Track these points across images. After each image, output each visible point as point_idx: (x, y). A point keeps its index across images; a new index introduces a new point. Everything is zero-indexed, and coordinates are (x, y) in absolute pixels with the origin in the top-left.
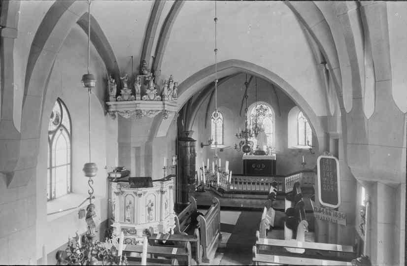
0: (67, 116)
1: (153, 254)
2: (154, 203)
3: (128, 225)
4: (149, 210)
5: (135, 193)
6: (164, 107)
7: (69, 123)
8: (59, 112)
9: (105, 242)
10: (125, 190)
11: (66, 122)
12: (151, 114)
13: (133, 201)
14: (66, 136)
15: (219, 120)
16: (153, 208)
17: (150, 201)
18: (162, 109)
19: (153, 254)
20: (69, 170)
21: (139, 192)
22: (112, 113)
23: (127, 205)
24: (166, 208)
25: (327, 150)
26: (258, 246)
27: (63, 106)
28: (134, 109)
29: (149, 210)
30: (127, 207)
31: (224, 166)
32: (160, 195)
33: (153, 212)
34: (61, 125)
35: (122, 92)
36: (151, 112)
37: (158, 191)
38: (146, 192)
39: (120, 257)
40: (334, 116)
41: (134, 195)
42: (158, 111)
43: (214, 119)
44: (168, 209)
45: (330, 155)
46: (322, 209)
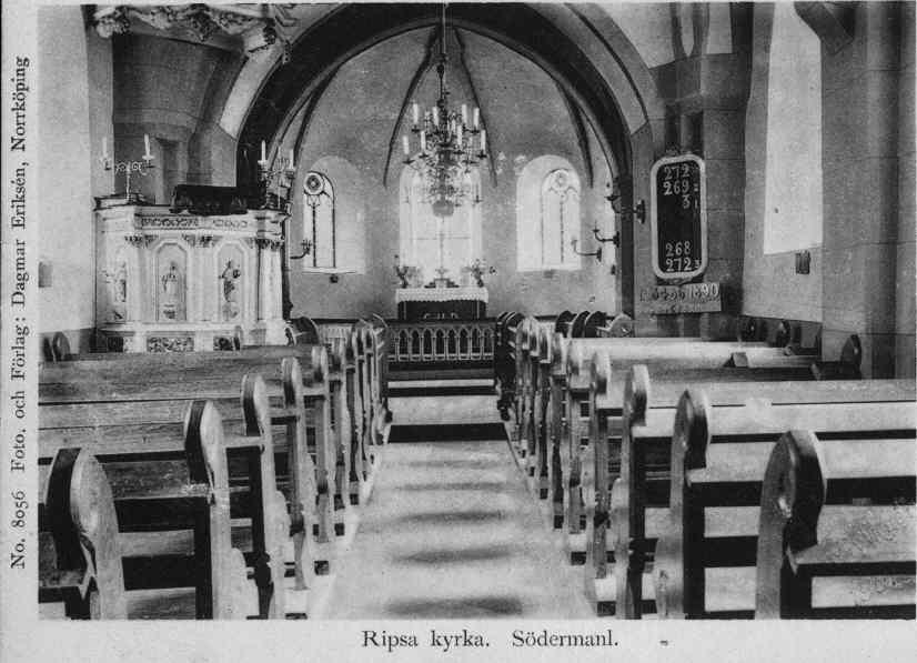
1: (392, 385)
4: (229, 287)
5: (190, 239)
10: (157, 232)
12: (230, 21)
13: (180, 263)
17: (229, 265)
19: (392, 385)
21: (199, 233)
22: (170, 482)
25: (672, 142)
26: (554, 376)
29: (229, 287)
31: (465, 139)
32: (254, 251)
36: (231, 17)
37: (248, 241)
38: (218, 239)
39: (572, 405)
40: (692, 56)
41: (187, 247)
45: (684, 153)
46: (661, 288)
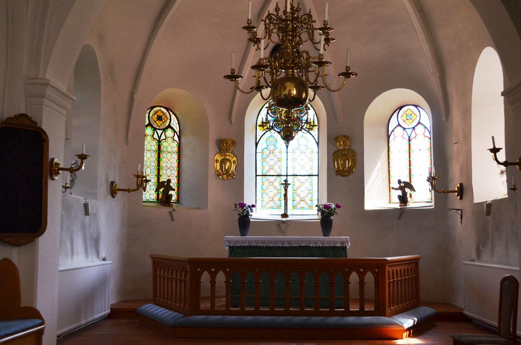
15: (169, 133)
43: (155, 129)
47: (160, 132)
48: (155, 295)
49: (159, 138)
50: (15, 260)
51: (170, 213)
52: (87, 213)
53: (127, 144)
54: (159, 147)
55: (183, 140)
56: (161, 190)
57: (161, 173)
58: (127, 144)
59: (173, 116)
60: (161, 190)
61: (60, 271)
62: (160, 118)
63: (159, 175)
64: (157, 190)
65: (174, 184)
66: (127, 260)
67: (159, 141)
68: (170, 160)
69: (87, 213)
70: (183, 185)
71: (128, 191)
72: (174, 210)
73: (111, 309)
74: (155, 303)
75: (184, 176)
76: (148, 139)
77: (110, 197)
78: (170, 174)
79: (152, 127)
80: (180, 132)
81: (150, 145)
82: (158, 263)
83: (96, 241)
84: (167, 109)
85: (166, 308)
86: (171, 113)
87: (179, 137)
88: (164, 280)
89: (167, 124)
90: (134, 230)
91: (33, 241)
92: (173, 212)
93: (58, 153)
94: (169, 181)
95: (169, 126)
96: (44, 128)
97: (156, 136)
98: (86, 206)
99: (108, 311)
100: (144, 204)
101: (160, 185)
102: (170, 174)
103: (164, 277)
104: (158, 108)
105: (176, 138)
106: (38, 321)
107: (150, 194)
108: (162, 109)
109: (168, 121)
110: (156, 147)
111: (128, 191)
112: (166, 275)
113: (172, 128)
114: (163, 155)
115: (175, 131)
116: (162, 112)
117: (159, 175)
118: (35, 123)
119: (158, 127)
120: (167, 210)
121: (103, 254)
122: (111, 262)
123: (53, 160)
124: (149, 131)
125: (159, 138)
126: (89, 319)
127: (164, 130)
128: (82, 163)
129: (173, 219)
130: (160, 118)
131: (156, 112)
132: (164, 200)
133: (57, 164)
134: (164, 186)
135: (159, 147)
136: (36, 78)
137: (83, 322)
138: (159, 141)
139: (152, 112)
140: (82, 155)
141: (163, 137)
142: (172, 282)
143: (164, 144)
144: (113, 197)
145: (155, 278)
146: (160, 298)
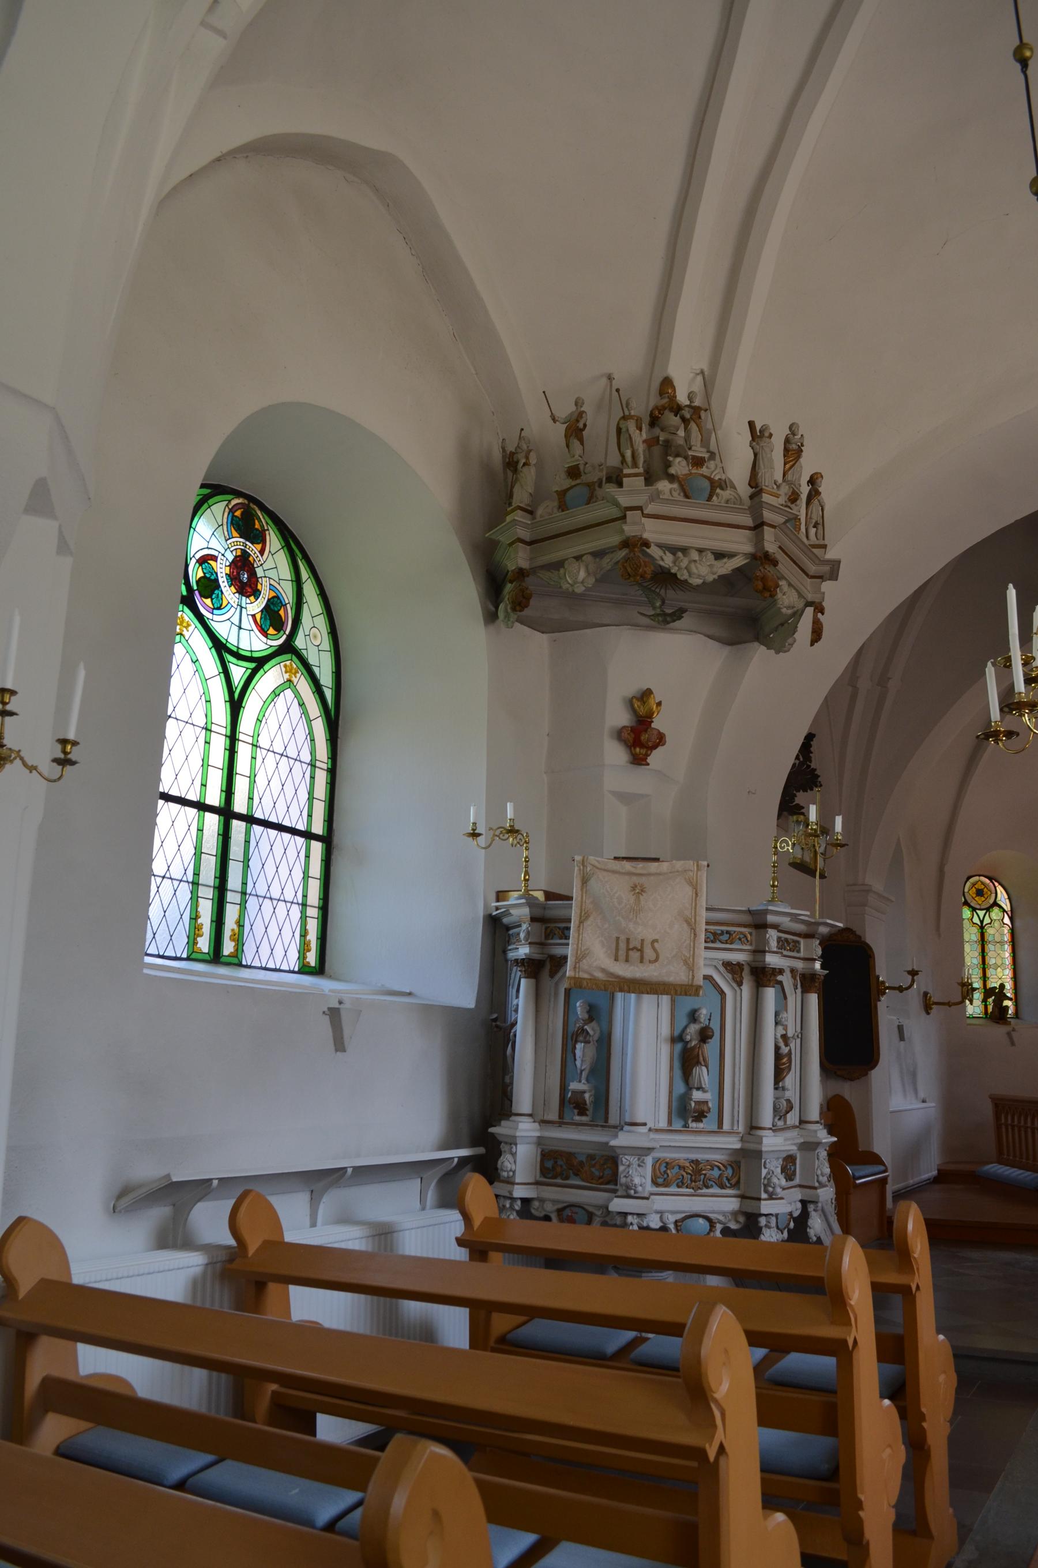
0: (322, 622)
2: (715, 1026)
3: (578, 1136)
6: (759, 540)
7: (326, 644)
8: (288, 594)
9: (764, 1419)
11: (313, 638)
14: (314, 708)
15: (996, 913)
16: (710, 1049)
18: (749, 548)
20: (316, 868)
23: (572, 1028)
24: (779, 1074)
27: (305, 574)
28: (615, 540)
30: (580, 1034)
32: (746, 989)
33: (703, 1075)
34: (288, 648)
35: (789, 1115)
42: (731, 555)
43: (974, 909)
44: (790, 1080)
47: (981, 913)
48: (1000, 1152)
49: (982, 922)
50: (847, 1097)
51: (1009, 1034)
52: (902, 1038)
53: (939, 935)
54: (982, 935)
55: (1017, 923)
56: (991, 1000)
57: (988, 974)
58: (939, 935)
59: (1000, 889)
60: (991, 1000)
61: (892, 1112)
62: (980, 893)
63: (985, 978)
64: (985, 1000)
65: (1009, 986)
66: (952, 1104)
67: (982, 927)
68: (1001, 956)
69: (902, 1038)
70: (1024, 990)
71: (949, 1004)
72: (1014, 1030)
73: (939, 1170)
74: (1000, 1163)
75: (1023, 978)
76: (966, 924)
77: (924, 1013)
78: (1002, 976)
79: (969, 906)
80: (1012, 910)
81: (971, 934)
82: (1002, 1106)
83: (914, 1075)
84: (990, 879)
85: (1020, 1168)
86: (996, 884)
87: (1011, 919)
88: (1013, 1130)
89: (991, 901)
90: (958, 1061)
91: (866, 1074)
92: (1014, 1034)
93: (884, 971)
94: (1002, 986)
95: (995, 904)
96: (868, 941)
97: (976, 920)
98: (900, 1028)
99: (935, 1173)
100: (969, 1021)
101: (988, 992)
102: (1002, 976)
103: (1013, 1127)
104: (976, 878)
105: (1007, 920)
106: (882, 1168)
107: (974, 1008)
108: (983, 879)
109: (993, 895)
110: (979, 935)
111: (949, 1004)
112: (1022, 1123)
113: (1000, 907)
114: (989, 947)
115: (1004, 911)
116: (983, 883)
117: (985, 978)
118: (860, 937)
119: (978, 907)
120: (1001, 1030)
121: (922, 1095)
122: (933, 1104)
123: (878, 977)
124: (967, 913)
125: (982, 922)
126: (917, 1179)
127: (988, 909)
128: (913, 981)
129: (1013, 1044)
130: (980, 893)
131: (974, 885)
132: (998, 1015)
133: (883, 982)
134: (998, 994)
135: (982, 935)
136: (855, 885)
137: (911, 1182)
138: (982, 927)
139: (968, 884)
140: (913, 970)
141: (987, 920)
142: (1026, 1132)
143: (990, 931)
144: (928, 1013)
145: (998, 1127)
146: (1008, 1155)
